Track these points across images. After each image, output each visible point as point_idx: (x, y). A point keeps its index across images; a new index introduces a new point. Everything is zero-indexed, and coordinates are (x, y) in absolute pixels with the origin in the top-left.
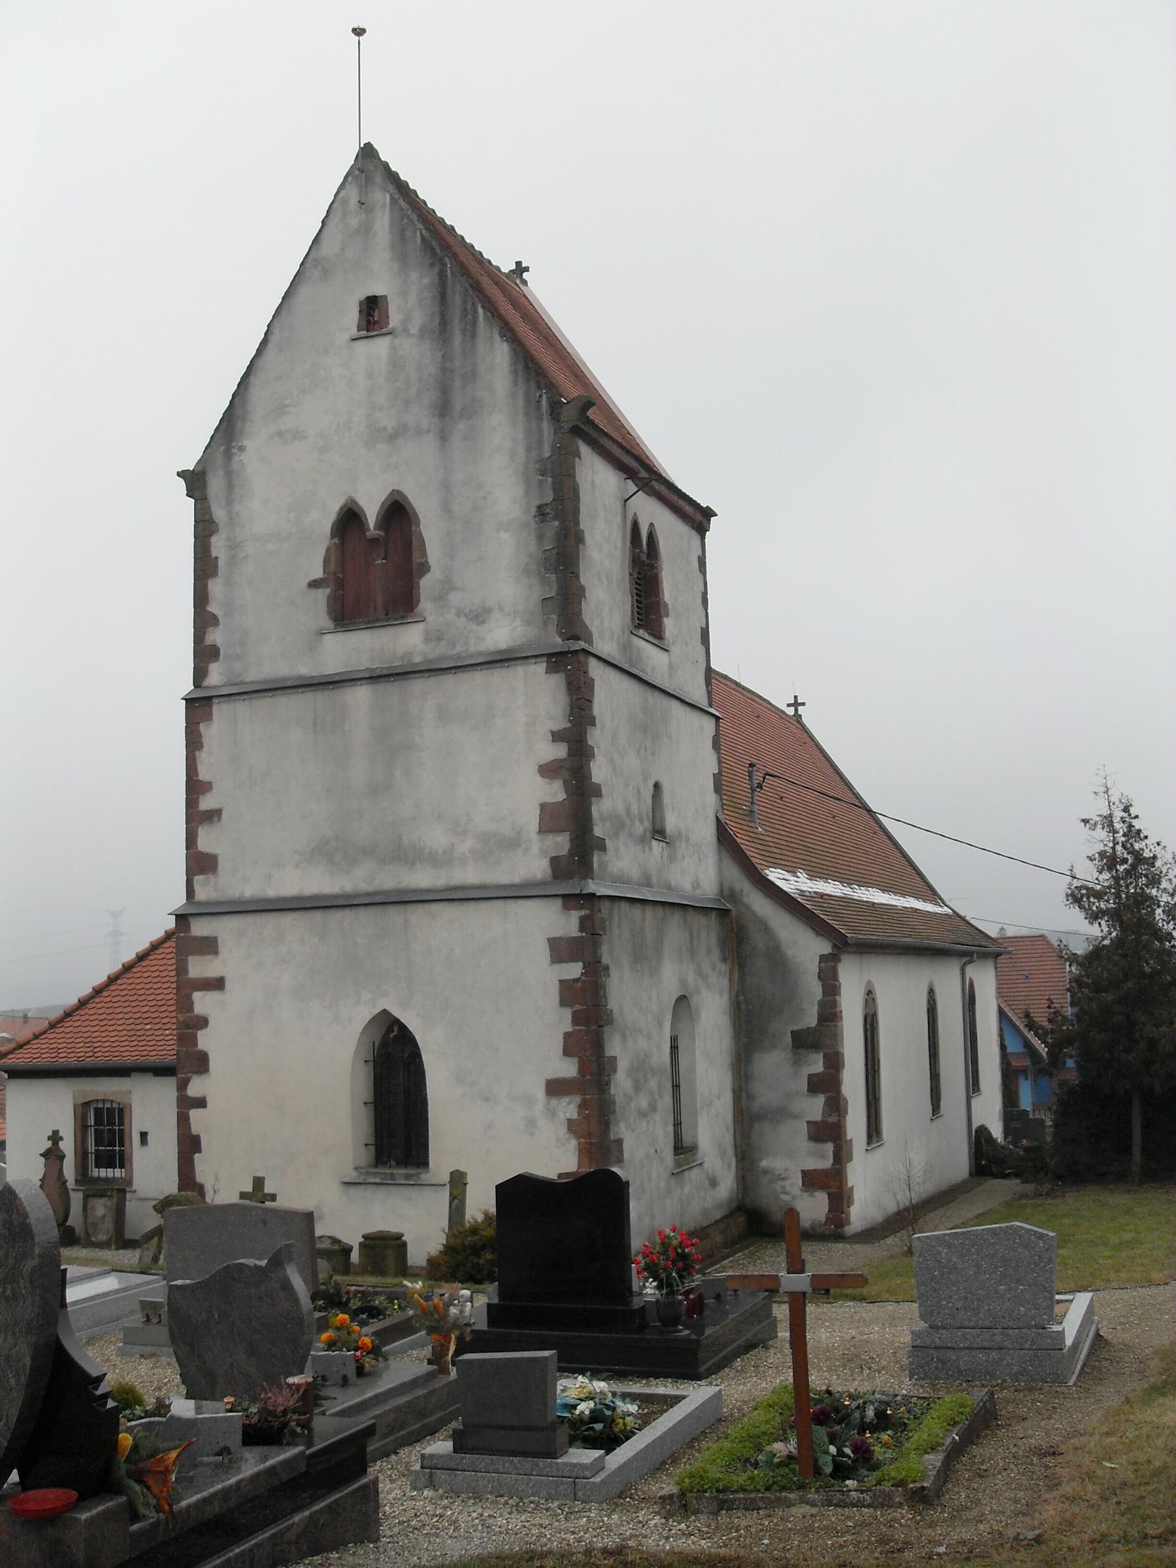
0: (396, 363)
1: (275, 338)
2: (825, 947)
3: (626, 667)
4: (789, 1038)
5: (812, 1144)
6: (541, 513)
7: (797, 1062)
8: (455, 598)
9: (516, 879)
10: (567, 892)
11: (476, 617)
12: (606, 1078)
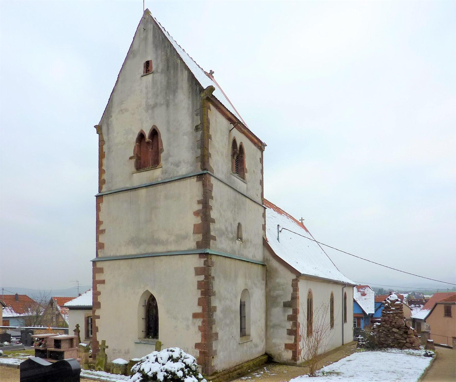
0: (154, 82)
1: (120, 79)
2: (294, 277)
3: (229, 184)
4: (282, 304)
5: (288, 336)
6: (197, 128)
7: (284, 311)
8: (171, 159)
9: (186, 249)
10: (200, 252)
11: (177, 165)
12: (211, 313)
